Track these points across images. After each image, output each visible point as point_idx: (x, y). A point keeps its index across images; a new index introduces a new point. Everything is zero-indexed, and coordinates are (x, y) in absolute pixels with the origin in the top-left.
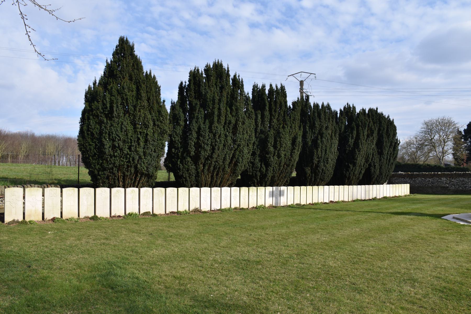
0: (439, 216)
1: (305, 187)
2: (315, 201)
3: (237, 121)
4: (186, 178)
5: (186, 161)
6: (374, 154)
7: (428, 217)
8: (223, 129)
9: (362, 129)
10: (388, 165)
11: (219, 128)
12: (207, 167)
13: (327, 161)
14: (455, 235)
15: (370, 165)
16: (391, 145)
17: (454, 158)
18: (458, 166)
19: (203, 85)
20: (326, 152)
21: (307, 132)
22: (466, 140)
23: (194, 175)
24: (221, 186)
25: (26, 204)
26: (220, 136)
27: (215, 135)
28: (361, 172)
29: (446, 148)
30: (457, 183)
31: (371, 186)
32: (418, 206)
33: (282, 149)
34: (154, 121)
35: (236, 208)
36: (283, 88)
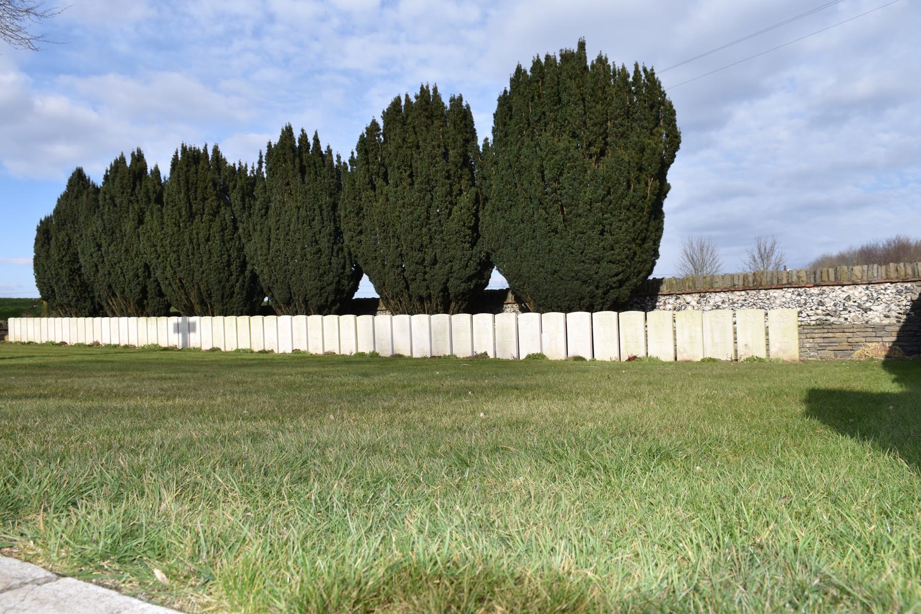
25: (21, 329)
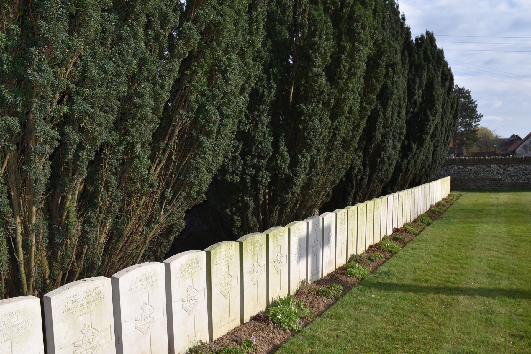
24: (108, 264)
30: (515, 172)
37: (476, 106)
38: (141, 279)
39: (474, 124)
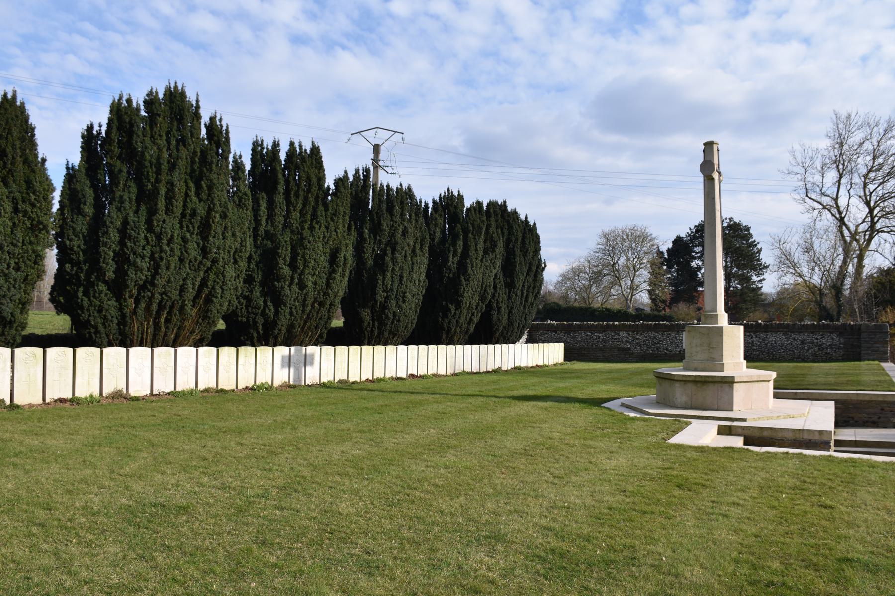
0: (597, 402)
1: (359, 347)
2: (379, 374)
3: (210, 210)
4: (96, 327)
5: (95, 291)
6: (498, 286)
7: (577, 405)
8: (177, 226)
9: (474, 239)
10: (524, 307)
11: (170, 225)
12: (143, 305)
13: (404, 297)
14: (613, 439)
15: (489, 307)
16: (529, 269)
17: (651, 299)
18: (656, 313)
19: (140, 133)
20: (401, 280)
21: (366, 240)
22: (670, 267)
23: (116, 321)
24: (175, 344)
26: (170, 241)
27: (159, 238)
28: (471, 320)
29: (637, 281)
30: (644, 341)
31: (491, 346)
32: (568, 384)
33: (307, 272)
34: (15, 202)
35: (207, 390)
36: (315, 150)
37: (759, 251)
38: (186, 353)
39: (755, 278)
